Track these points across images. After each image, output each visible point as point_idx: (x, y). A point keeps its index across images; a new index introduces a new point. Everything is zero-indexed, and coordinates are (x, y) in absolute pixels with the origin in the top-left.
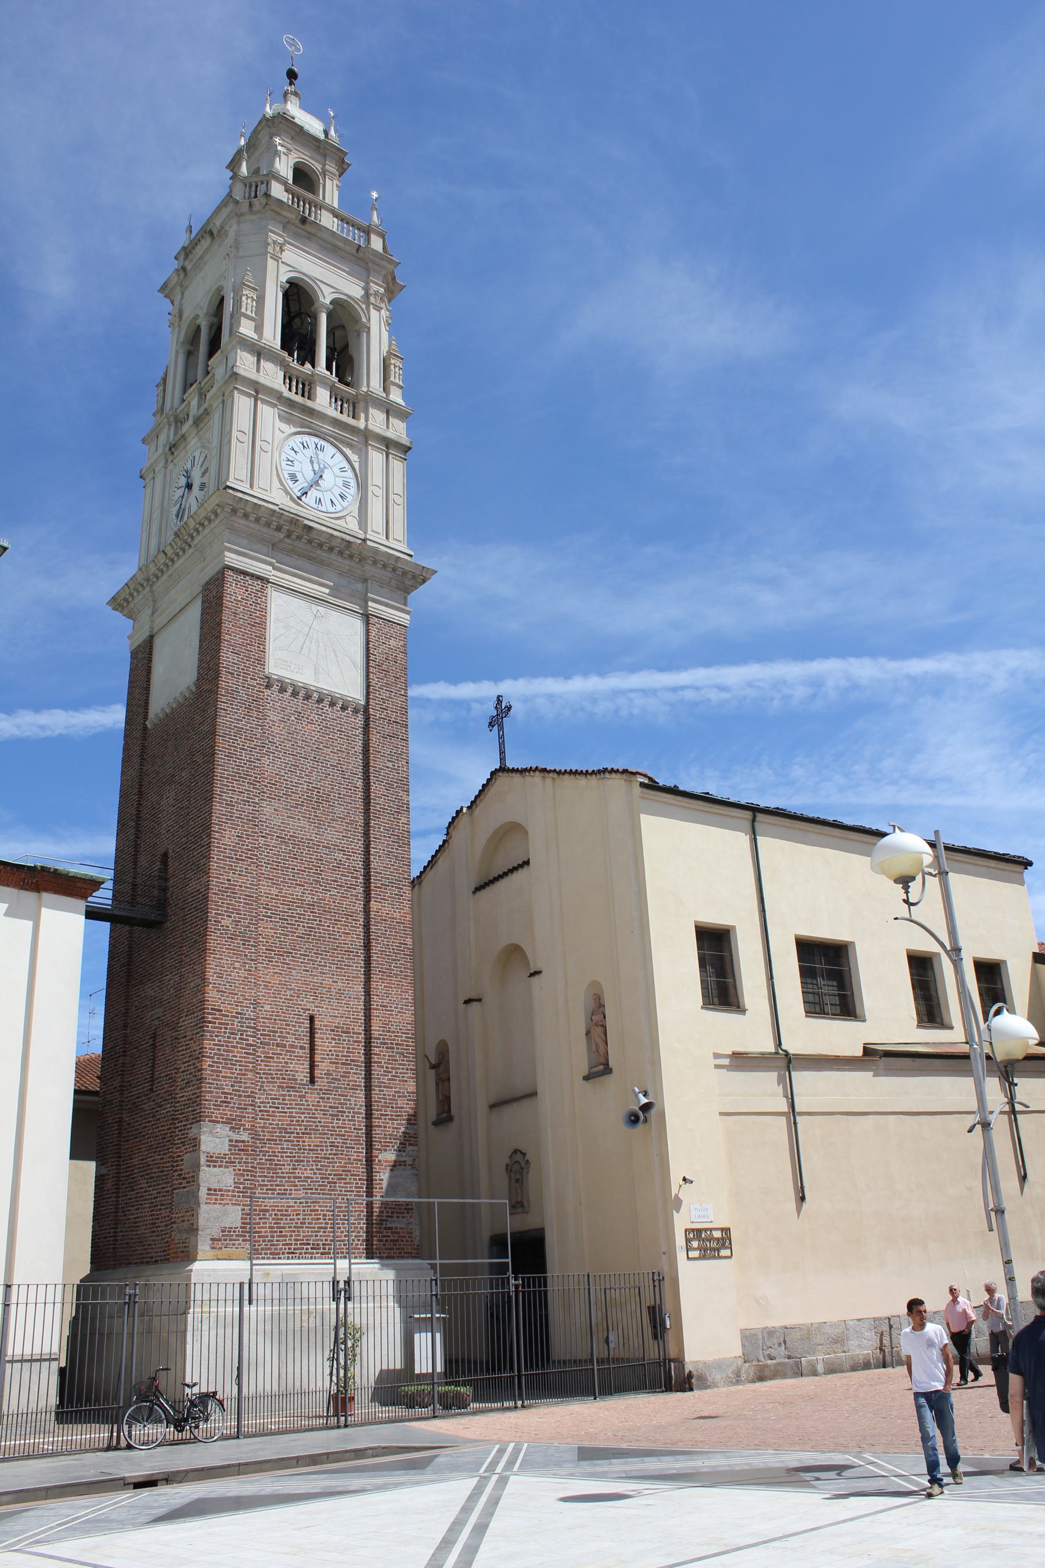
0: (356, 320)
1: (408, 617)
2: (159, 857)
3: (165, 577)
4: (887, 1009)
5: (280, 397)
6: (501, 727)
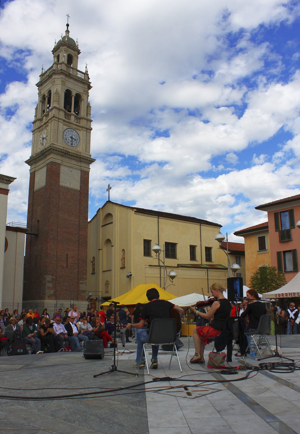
2: (37, 221)
4: (183, 256)
5: (64, 121)
6: (109, 192)
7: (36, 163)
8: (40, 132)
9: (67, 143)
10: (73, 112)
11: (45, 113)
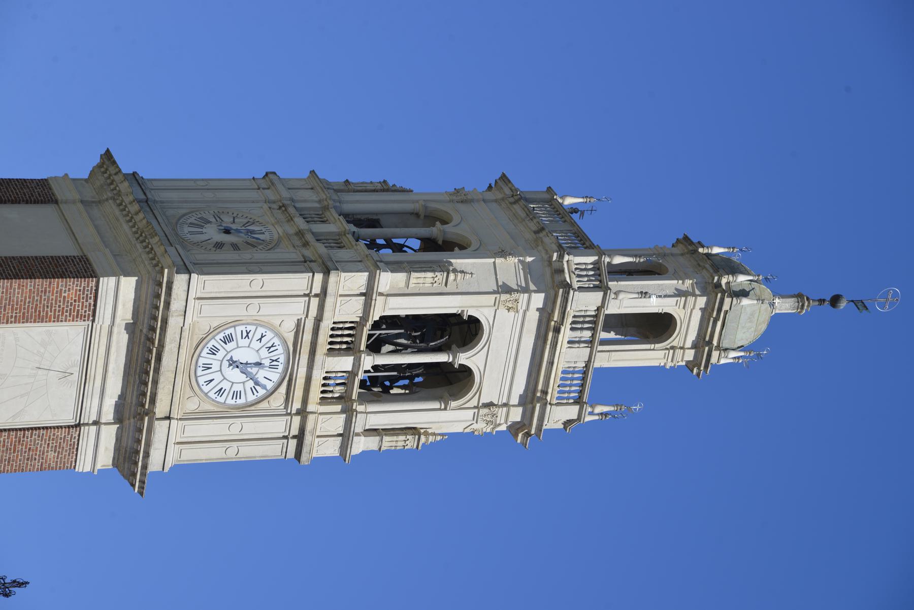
0: (456, 396)
3: (117, 212)
10: (368, 361)
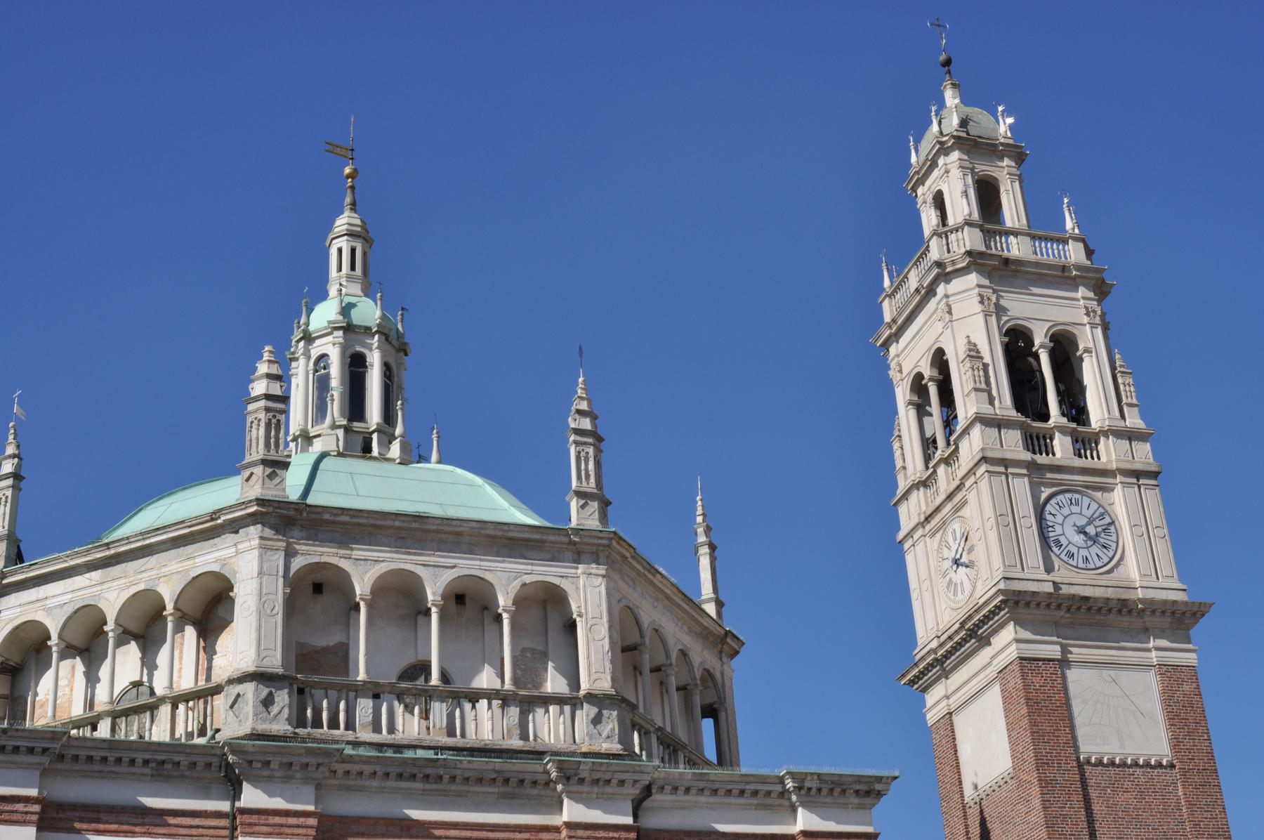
1: (1193, 655)
7: (946, 674)
8: (933, 535)
9: (1066, 559)
11: (939, 453)
